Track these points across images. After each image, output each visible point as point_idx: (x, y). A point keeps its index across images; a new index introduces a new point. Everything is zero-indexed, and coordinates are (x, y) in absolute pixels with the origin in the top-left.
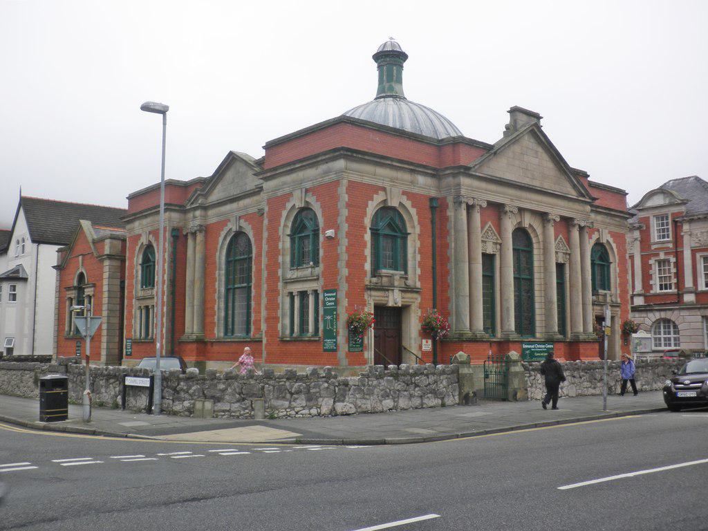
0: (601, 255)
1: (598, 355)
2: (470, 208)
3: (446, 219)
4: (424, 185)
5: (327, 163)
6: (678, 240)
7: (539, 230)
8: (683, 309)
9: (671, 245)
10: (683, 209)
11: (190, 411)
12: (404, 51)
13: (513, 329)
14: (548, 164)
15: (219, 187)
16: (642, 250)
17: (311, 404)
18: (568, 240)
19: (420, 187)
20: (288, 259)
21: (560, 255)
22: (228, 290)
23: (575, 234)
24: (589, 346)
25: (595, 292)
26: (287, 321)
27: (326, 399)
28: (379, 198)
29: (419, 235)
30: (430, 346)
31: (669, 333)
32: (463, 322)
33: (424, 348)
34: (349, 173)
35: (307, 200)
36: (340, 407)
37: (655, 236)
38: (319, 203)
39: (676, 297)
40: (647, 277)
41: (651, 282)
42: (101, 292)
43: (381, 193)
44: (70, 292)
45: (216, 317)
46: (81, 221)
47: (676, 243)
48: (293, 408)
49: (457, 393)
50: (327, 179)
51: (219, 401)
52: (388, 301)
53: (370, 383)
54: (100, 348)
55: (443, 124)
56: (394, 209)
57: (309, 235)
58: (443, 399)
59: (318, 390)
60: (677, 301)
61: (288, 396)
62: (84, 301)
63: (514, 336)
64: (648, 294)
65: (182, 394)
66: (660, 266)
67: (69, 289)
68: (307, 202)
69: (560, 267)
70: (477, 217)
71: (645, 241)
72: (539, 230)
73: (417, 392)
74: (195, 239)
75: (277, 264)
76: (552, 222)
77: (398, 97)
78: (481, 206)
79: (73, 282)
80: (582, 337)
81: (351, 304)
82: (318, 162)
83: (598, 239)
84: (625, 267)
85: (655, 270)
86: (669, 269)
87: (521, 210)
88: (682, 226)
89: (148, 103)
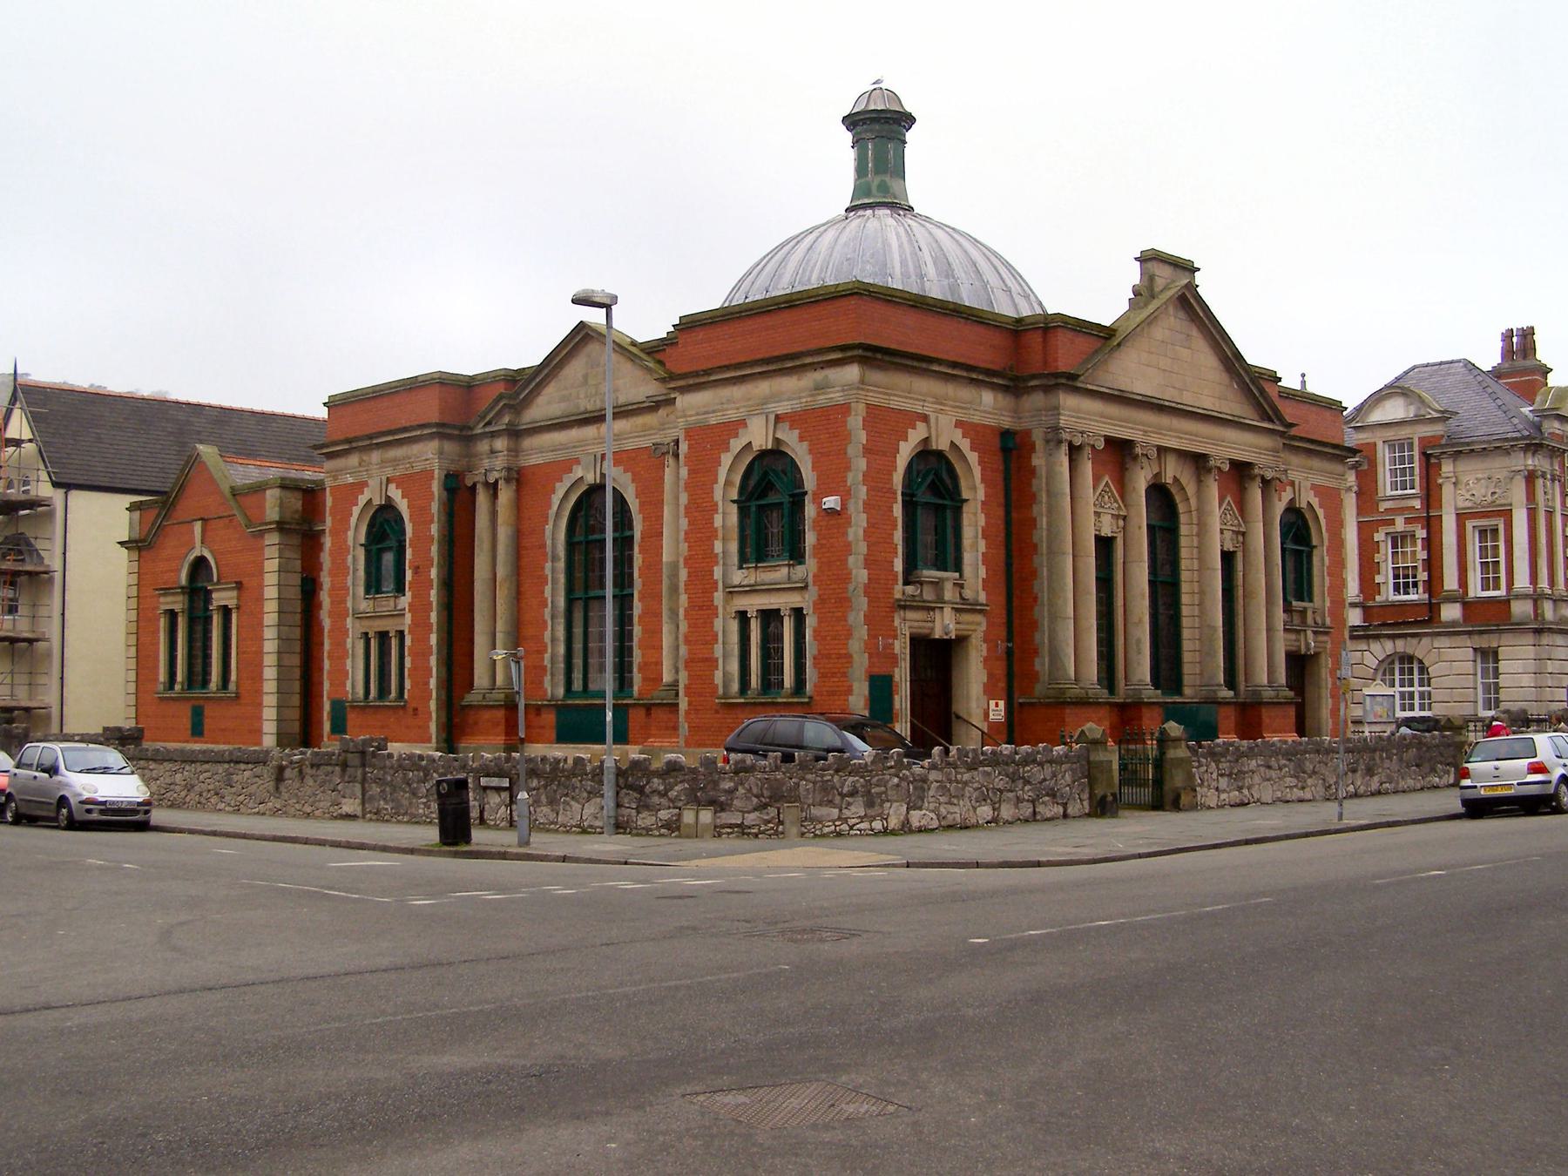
0: (1297, 529)
1: (1294, 728)
2: (1074, 451)
3: (1033, 472)
4: (988, 406)
5: (822, 368)
6: (1431, 495)
7: (1191, 489)
8: (1439, 634)
9: (1417, 504)
10: (1438, 429)
11: (673, 827)
12: (908, 109)
13: (1148, 679)
14: (1207, 360)
15: (550, 391)
16: (1360, 511)
17: (871, 812)
18: (1242, 505)
19: (985, 412)
20: (734, 547)
21: (1228, 535)
22: (570, 602)
23: (1256, 494)
24: (21, 687)
25: (1288, 609)
26: (734, 667)
27: (895, 805)
28: (916, 436)
29: (983, 503)
30: (1003, 714)
31: (1411, 685)
32: (1065, 670)
33: (991, 717)
34: (868, 390)
35: (779, 435)
36: (916, 818)
37: (1385, 484)
38: (805, 444)
39: (1426, 609)
40: (1368, 568)
41: (1378, 579)
42: (260, 600)
43: (921, 426)
44: (170, 599)
45: (547, 656)
46: (197, 445)
47: (1428, 501)
48: (845, 820)
49: (1086, 796)
50: (822, 400)
51: (723, 810)
52: (933, 629)
53: (959, 777)
54: (260, 718)
55: (995, 268)
56: (940, 455)
57: (782, 503)
58: (1065, 805)
59: (883, 789)
60: (1427, 615)
61: (837, 799)
62: (211, 617)
63: (1151, 694)
64: (1370, 603)
65: (656, 799)
66: (1394, 546)
67: (166, 591)
68: (777, 441)
69: (1228, 557)
70: (1087, 468)
71: (1367, 494)
72: (1191, 489)
73: (1028, 792)
74: (495, 496)
75: (712, 559)
76: (1215, 472)
77: (900, 207)
78: (1093, 446)
79: (179, 577)
80: (1268, 694)
81: (873, 636)
82: (804, 366)
83: (1292, 501)
84: (1341, 554)
85: (1386, 555)
86: (1414, 553)
87: (1162, 450)
88: (1439, 466)
89: (578, 293)
